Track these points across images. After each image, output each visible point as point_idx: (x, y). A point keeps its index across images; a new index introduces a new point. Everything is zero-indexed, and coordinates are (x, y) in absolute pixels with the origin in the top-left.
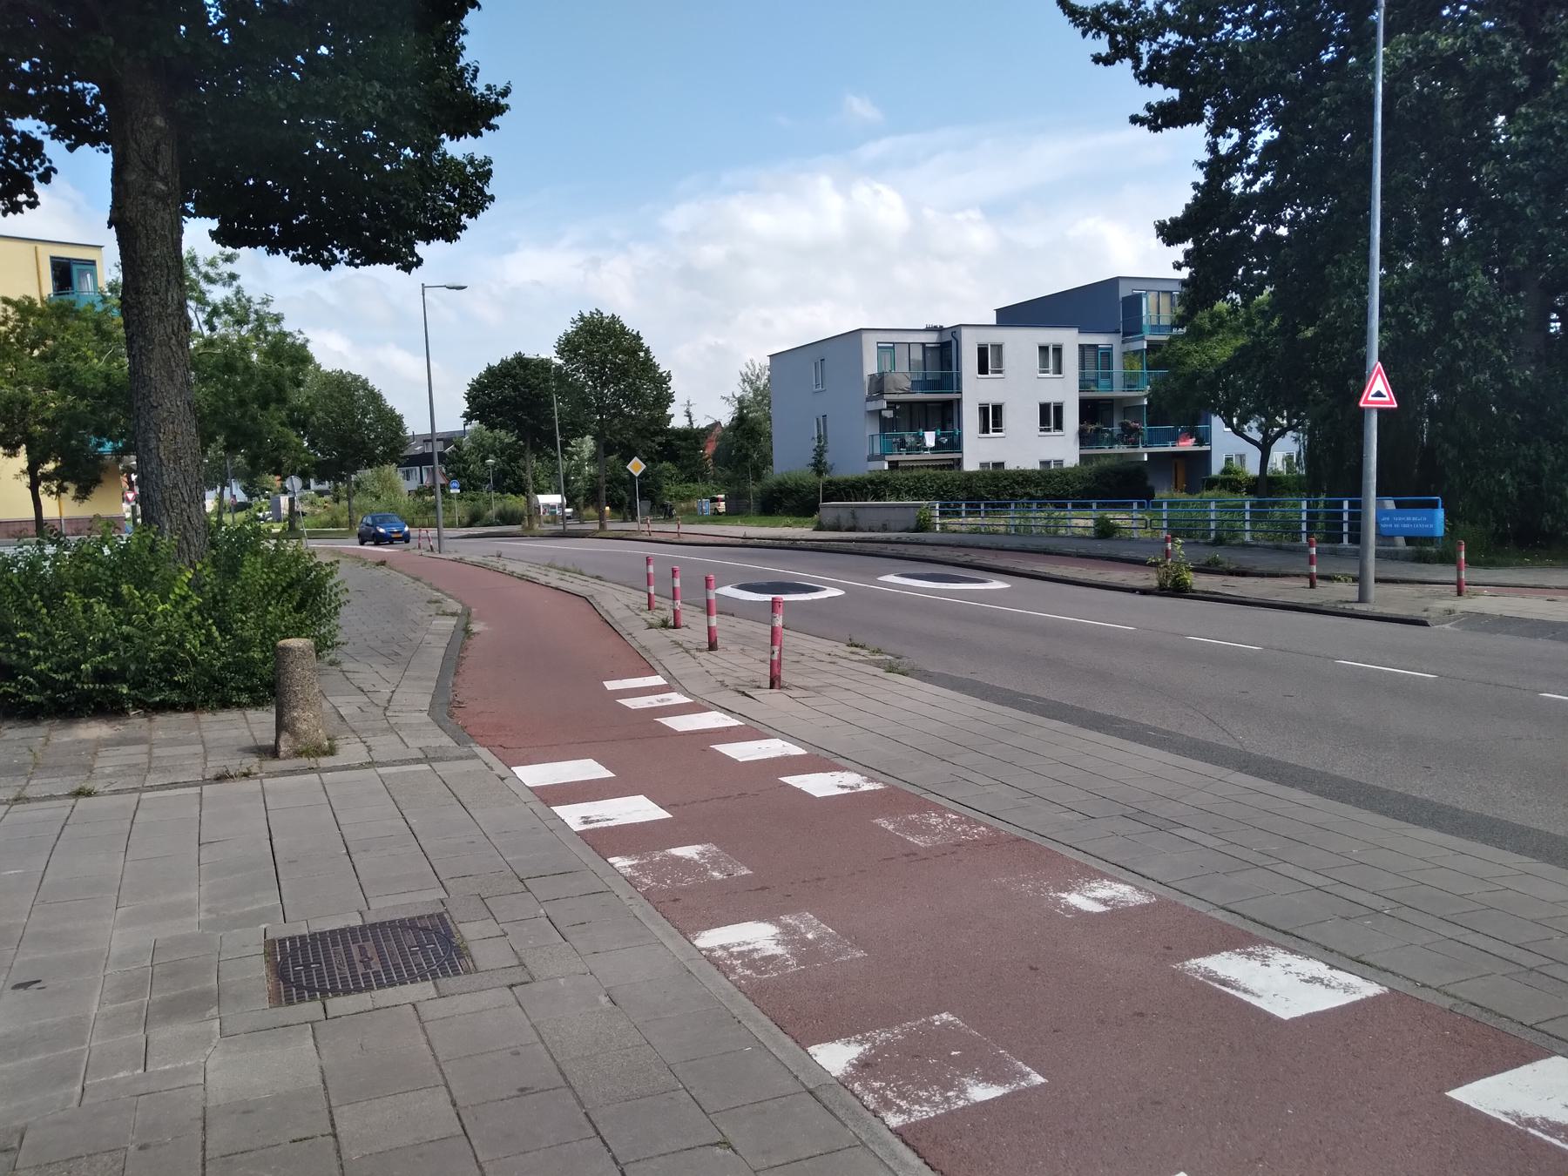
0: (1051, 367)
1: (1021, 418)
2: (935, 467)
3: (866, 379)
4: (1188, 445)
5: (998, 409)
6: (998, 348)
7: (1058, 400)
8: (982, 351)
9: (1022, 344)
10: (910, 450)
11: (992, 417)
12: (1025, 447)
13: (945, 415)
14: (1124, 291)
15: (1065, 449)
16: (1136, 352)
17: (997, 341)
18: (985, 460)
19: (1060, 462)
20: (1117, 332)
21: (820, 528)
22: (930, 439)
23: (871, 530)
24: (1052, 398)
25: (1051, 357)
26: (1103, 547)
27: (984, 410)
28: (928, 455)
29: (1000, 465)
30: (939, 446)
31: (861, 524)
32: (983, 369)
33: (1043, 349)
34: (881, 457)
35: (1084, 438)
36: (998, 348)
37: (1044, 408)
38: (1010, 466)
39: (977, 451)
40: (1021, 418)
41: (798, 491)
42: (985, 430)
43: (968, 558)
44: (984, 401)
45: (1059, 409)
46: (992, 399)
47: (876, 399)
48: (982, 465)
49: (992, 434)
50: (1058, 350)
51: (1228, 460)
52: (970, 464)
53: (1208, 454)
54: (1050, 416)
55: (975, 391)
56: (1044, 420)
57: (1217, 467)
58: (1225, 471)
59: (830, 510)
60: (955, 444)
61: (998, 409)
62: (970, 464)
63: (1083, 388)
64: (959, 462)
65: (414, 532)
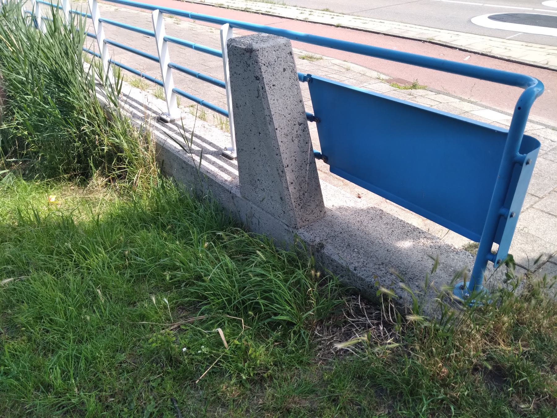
65: (324, 58)
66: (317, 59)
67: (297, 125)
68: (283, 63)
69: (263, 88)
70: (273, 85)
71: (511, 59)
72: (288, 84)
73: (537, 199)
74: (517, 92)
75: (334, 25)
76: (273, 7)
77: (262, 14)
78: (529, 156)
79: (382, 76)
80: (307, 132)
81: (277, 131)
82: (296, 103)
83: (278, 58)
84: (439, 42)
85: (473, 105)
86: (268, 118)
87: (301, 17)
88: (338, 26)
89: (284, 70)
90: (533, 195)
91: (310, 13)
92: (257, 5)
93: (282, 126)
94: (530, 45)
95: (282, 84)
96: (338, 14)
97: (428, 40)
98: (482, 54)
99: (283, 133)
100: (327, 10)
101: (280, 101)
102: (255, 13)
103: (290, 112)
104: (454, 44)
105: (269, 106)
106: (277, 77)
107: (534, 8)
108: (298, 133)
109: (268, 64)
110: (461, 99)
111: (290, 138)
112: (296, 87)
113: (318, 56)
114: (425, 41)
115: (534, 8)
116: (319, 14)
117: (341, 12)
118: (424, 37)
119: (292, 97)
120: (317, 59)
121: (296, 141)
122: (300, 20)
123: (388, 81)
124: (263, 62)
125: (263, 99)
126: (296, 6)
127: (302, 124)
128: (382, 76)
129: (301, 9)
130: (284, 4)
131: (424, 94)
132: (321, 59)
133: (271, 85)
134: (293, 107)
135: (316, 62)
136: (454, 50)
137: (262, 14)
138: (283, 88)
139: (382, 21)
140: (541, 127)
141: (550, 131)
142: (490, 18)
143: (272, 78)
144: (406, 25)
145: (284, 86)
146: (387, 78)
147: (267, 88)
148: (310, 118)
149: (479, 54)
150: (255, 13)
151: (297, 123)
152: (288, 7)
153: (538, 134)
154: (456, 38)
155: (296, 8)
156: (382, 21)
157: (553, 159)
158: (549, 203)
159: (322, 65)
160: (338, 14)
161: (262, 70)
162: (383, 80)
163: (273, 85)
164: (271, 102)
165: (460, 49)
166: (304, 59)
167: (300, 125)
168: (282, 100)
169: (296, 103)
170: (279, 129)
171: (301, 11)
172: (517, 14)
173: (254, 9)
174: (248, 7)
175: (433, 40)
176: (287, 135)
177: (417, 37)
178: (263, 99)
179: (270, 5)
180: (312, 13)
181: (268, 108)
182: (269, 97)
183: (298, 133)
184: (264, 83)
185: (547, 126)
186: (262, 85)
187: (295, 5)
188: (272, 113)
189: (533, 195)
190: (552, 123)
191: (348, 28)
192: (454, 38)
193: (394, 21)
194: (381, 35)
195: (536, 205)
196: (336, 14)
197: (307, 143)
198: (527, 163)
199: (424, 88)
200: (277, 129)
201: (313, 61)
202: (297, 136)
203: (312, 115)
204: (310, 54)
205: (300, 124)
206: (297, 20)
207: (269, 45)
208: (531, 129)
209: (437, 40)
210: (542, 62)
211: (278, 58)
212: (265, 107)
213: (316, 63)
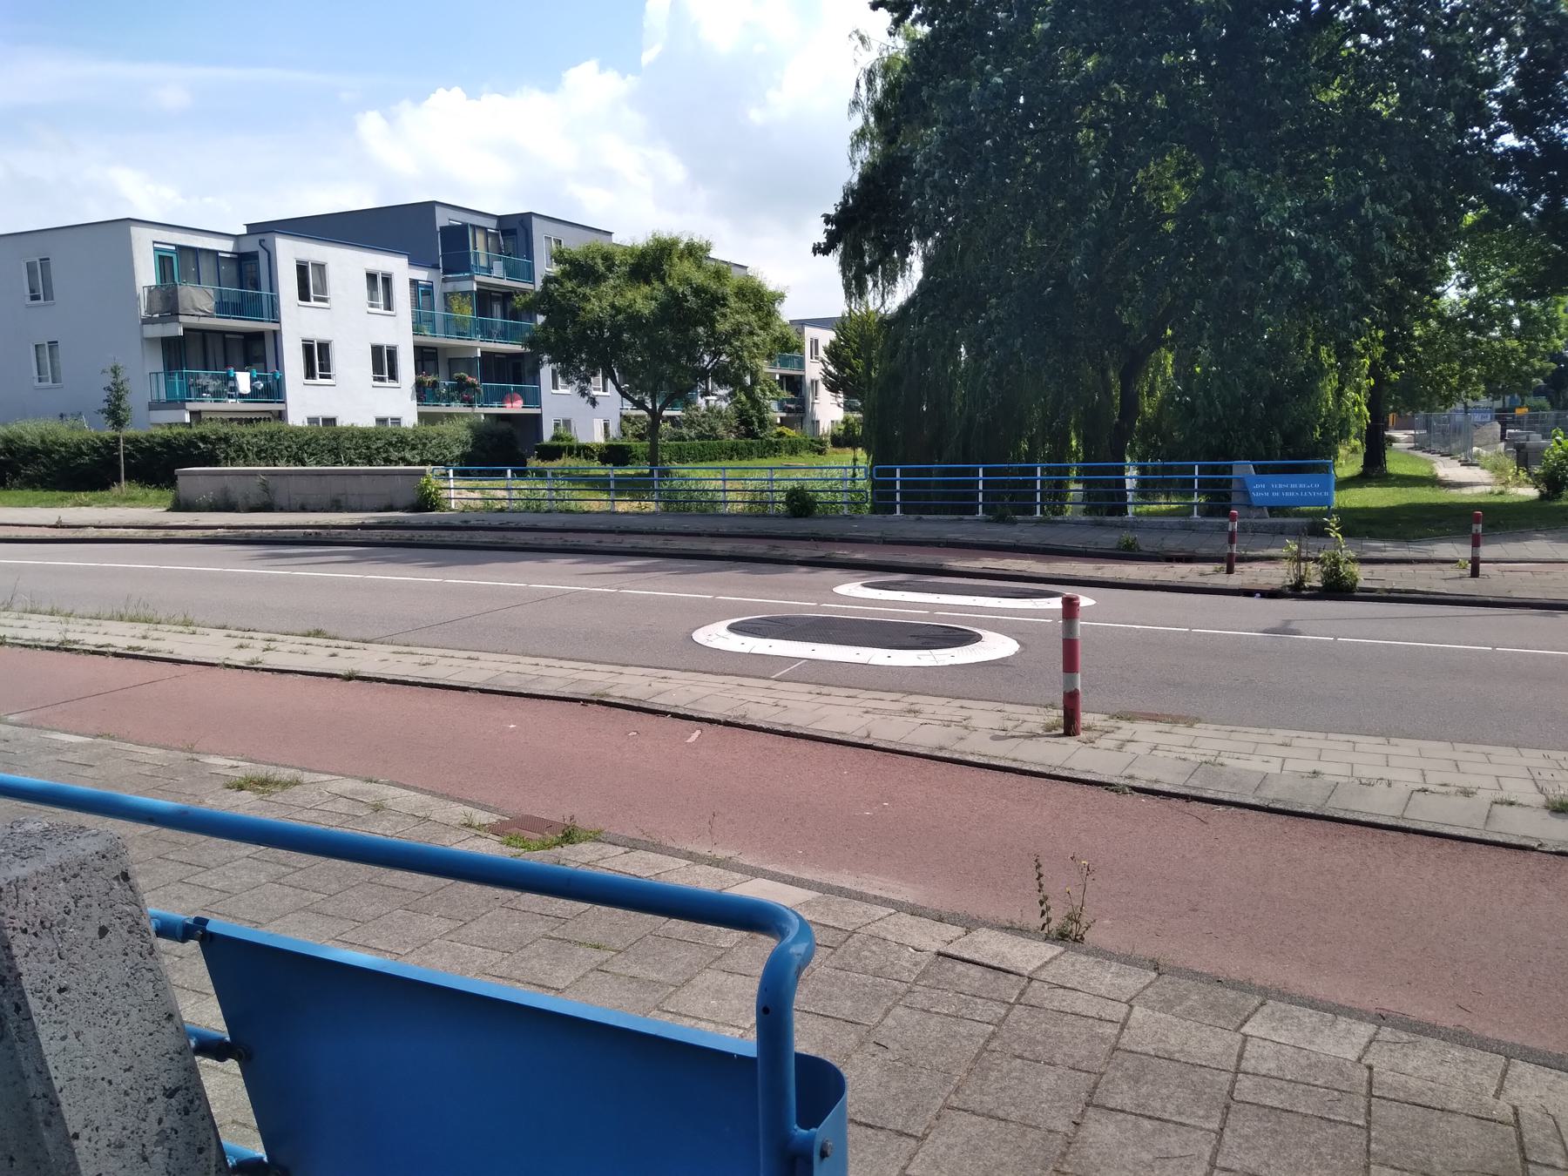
0: (381, 302)
1: (351, 363)
2: (240, 421)
3: (143, 295)
4: (516, 407)
5: (324, 348)
6: (320, 268)
7: (391, 343)
8: (302, 269)
9: (347, 266)
10: (217, 395)
11: (318, 358)
12: (359, 400)
13: (256, 349)
14: (442, 219)
15: (398, 403)
16: (464, 294)
17: (319, 259)
18: (313, 414)
19: (397, 421)
20: (436, 267)
21: (179, 506)
22: (243, 381)
23: (303, 509)
24: (385, 341)
25: (379, 284)
26: (803, 526)
27: (308, 348)
28: (232, 404)
29: (330, 421)
30: (255, 395)
31: (280, 499)
32: (304, 295)
33: (371, 277)
34: (179, 404)
35: (423, 392)
36: (320, 268)
37: (377, 351)
38: (343, 422)
39: (304, 402)
40: (351, 363)
41: (48, 452)
42: (310, 374)
43: (821, 554)
44: (309, 336)
45: (392, 353)
46: (318, 335)
47: (162, 320)
48: (312, 420)
49: (319, 381)
50: (387, 280)
51: (557, 425)
52: (297, 417)
53: (538, 417)
54: (383, 362)
55: (297, 323)
56: (378, 368)
57: (547, 434)
58: (555, 438)
59: (193, 478)
60: (273, 390)
61: (324, 348)
62: (297, 417)
63: (417, 331)
64: (281, 416)
65: (307, 777)
66: (285, 785)
67: (161, 1099)
68: (96, 911)
69: (18, 1008)
70: (61, 991)
71: (793, 730)
72: (118, 972)
73: (913, 1142)
74: (754, 951)
75: (337, 676)
76: (156, 635)
77: (116, 655)
78: (822, 1133)
79: (482, 817)
80: (202, 1112)
81: (80, 1145)
82: (153, 1028)
83: (77, 899)
84: (622, 702)
85: (721, 871)
86: (40, 1106)
87: (240, 658)
88: (349, 678)
89: (103, 931)
90: (900, 1134)
91: (264, 645)
92: (102, 630)
93: (99, 1119)
94: (825, 690)
95: (95, 977)
96: (348, 644)
97: (595, 698)
98: (727, 724)
99: (104, 1142)
100: (318, 634)
101: (90, 1035)
102: (94, 653)
103: (127, 1062)
104: (660, 702)
105: (43, 1062)
106: (75, 959)
107: (819, 602)
108: (166, 1124)
109: (38, 927)
110: (690, 856)
111: (131, 1151)
112: (150, 975)
113: (285, 774)
114: (586, 702)
115: (819, 602)
116: (295, 647)
117: (358, 634)
118: (584, 691)
119: (134, 1012)
120: (285, 785)
121: (159, 1157)
122: (237, 667)
123: (495, 830)
124: (17, 924)
125: (19, 1046)
126: (224, 628)
127: (177, 1090)
128: (482, 817)
129: (240, 633)
130: (187, 624)
131: (594, 857)
132: (298, 783)
133: (54, 993)
134: (140, 1044)
135: (280, 796)
136: (662, 719)
137: (116, 655)
138: (100, 989)
139: (474, 654)
140: (882, 911)
141: (906, 919)
142: (732, 628)
143: (58, 969)
144: (535, 660)
145: (105, 982)
146: (493, 818)
147: (34, 1004)
148: (214, 1049)
149: (719, 722)
150: (94, 653)
151: (158, 1092)
152: (199, 630)
153: (882, 934)
154: (662, 686)
155: (226, 632)
156: (474, 654)
157: (926, 1004)
158: (943, 1149)
159: (300, 801)
160: (348, 644)
161: (15, 951)
162: (481, 827)
163: (61, 991)
164: (50, 1047)
165: (675, 715)
166: (241, 788)
167: (170, 1096)
168: (97, 1031)
169: (153, 1028)
170: (85, 1133)
171: (237, 642)
172: (787, 618)
173: (91, 640)
174: (70, 636)
175: (608, 695)
176: (121, 1146)
177: (567, 692)
178: (19, 1046)
179: (141, 628)
180: (272, 645)
181: (42, 1072)
182: (45, 1033)
183: (166, 1124)
184: (22, 992)
185: (899, 907)
186: (16, 999)
187: (219, 623)
188: (57, 1084)
189: (900, 1134)
190: (907, 893)
191: (379, 680)
192: (658, 686)
193: (505, 652)
194: (472, 694)
195: (913, 1165)
196: (342, 643)
197: (201, 1150)
198: (824, 1155)
199: (596, 837)
200: (76, 1136)
201: (271, 793)
202: (163, 1137)
203: (222, 1040)
204: (262, 771)
205: (170, 1094)
206: (228, 666)
207: (41, 868)
208: (866, 921)
209: (616, 695)
210: (858, 733)
211: (77, 899)
212: (28, 1068)
213: (280, 799)
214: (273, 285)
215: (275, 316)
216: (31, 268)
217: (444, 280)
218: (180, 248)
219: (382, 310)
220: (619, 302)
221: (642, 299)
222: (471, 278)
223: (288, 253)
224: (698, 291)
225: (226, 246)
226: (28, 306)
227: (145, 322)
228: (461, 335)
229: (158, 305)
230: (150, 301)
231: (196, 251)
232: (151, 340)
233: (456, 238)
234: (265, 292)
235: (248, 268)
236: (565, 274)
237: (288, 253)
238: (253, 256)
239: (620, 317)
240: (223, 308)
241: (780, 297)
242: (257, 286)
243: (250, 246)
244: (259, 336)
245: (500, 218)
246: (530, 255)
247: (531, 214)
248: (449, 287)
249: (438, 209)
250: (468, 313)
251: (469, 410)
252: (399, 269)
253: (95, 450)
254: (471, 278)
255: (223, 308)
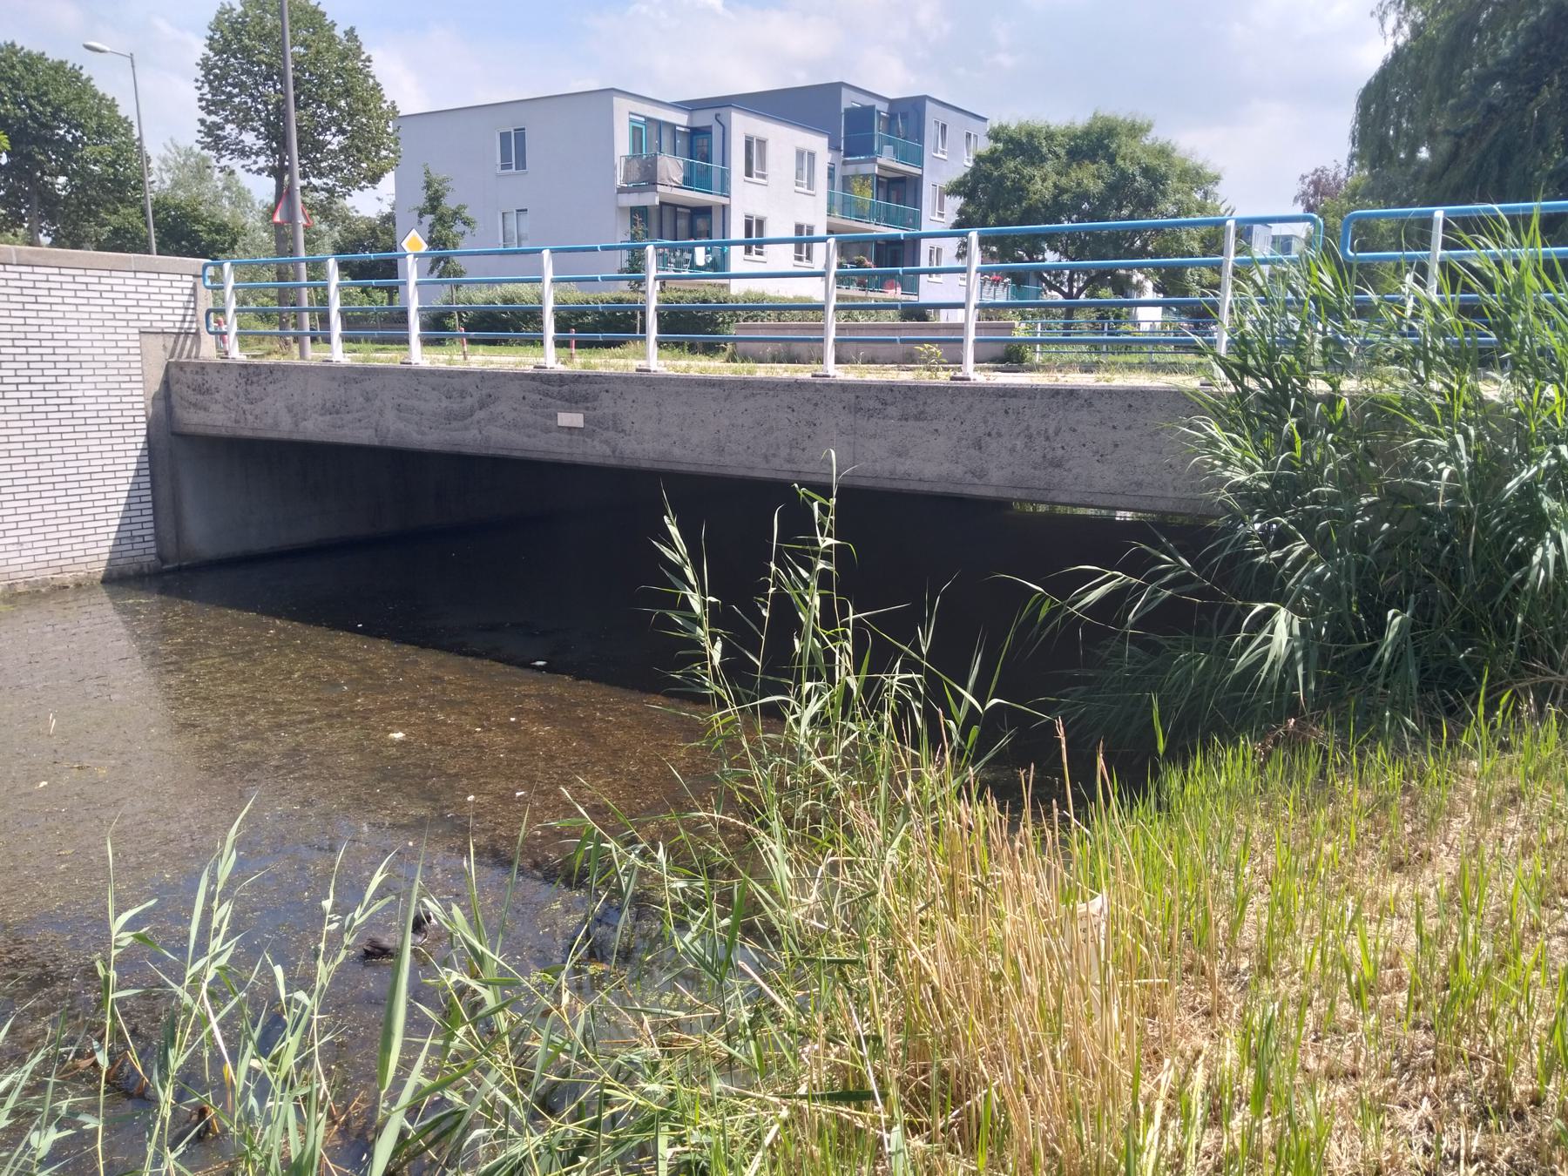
6: (762, 143)
9: (784, 141)
13: (698, 222)
14: (848, 101)
16: (866, 177)
22: (701, 256)
33: (800, 154)
36: (762, 143)
44: (750, 213)
46: (757, 212)
47: (637, 189)
50: (812, 155)
55: (744, 199)
60: (718, 265)
214: (725, 160)
215: (725, 190)
216: (505, 137)
217: (845, 163)
218: (648, 119)
219: (804, 190)
220: (1063, 181)
221: (1090, 178)
222: (874, 161)
223: (742, 125)
224: (1147, 172)
225: (681, 119)
226: (498, 176)
227: (621, 190)
228: (860, 217)
229: (636, 175)
230: (627, 171)
231: (660, 124)
232: (622, 209)
233: (860, 120)
234: (715, 165)
235: (700, 141)
236: (1007, 152)
237: (742, 125)
238: (705, 132)
239: (1065, 197)
240: (688, 182)
241: (1216, 179)
242: (707, 158)
243: (704, 119)
244: (705, 211)
245: (892, 102)
246: (921, 139)
247: (924, 98)
248: (851, 170)
249: (844, 91)
250: (868, 196)
251: (863, 294)
252: (818, 144)
253: (596, 311)
254: (874, 161)
255: (688, 182)
